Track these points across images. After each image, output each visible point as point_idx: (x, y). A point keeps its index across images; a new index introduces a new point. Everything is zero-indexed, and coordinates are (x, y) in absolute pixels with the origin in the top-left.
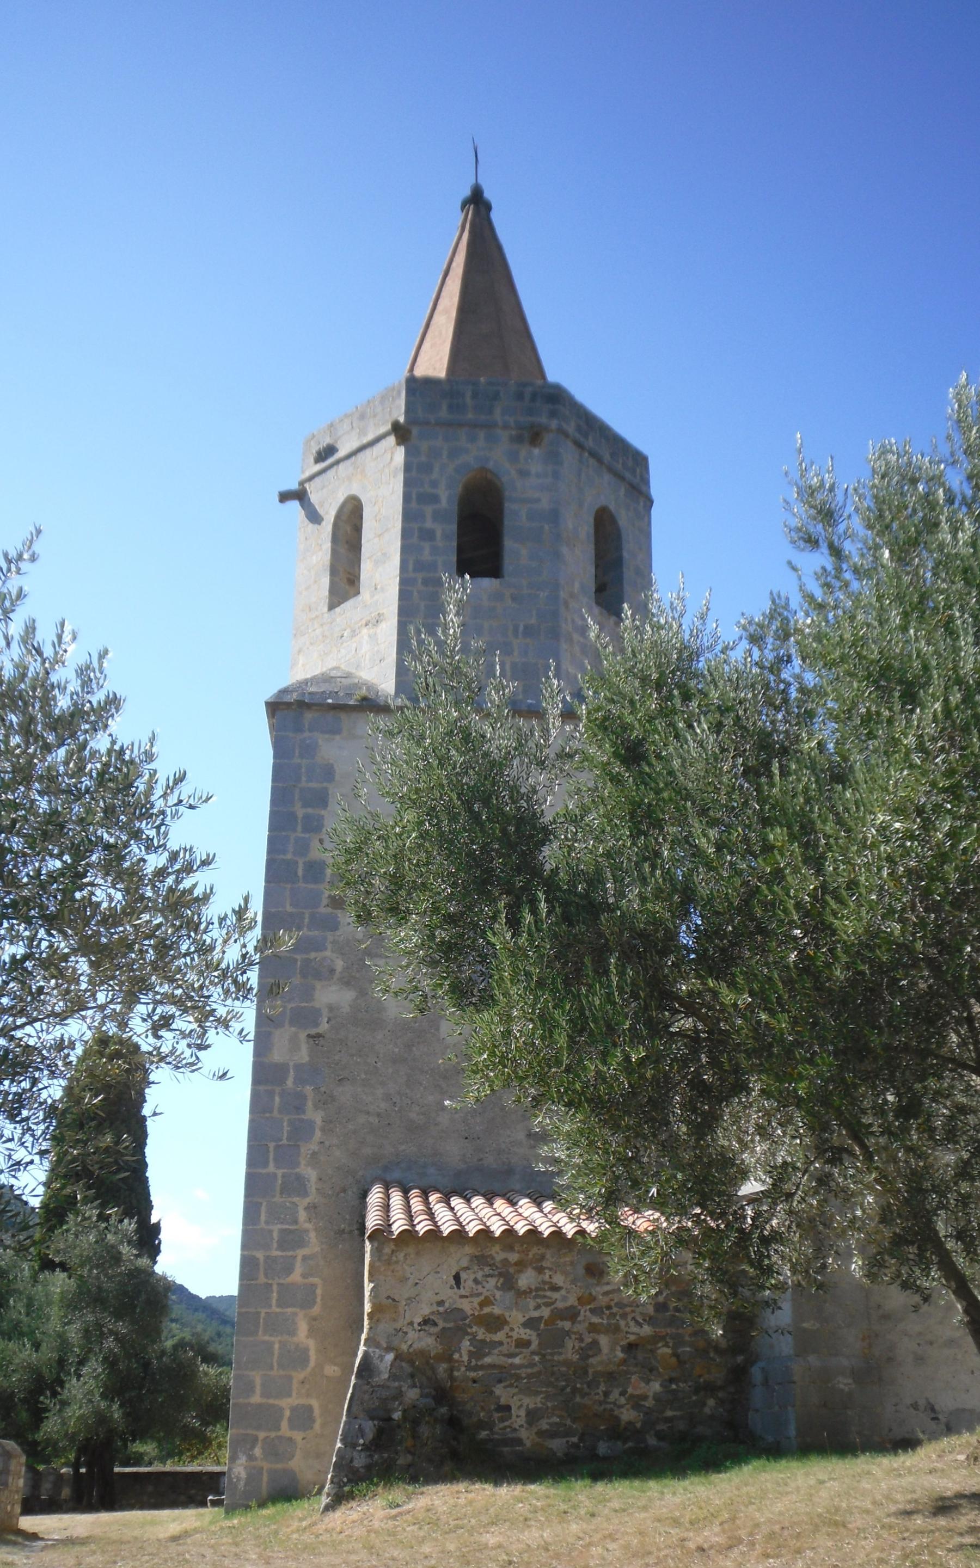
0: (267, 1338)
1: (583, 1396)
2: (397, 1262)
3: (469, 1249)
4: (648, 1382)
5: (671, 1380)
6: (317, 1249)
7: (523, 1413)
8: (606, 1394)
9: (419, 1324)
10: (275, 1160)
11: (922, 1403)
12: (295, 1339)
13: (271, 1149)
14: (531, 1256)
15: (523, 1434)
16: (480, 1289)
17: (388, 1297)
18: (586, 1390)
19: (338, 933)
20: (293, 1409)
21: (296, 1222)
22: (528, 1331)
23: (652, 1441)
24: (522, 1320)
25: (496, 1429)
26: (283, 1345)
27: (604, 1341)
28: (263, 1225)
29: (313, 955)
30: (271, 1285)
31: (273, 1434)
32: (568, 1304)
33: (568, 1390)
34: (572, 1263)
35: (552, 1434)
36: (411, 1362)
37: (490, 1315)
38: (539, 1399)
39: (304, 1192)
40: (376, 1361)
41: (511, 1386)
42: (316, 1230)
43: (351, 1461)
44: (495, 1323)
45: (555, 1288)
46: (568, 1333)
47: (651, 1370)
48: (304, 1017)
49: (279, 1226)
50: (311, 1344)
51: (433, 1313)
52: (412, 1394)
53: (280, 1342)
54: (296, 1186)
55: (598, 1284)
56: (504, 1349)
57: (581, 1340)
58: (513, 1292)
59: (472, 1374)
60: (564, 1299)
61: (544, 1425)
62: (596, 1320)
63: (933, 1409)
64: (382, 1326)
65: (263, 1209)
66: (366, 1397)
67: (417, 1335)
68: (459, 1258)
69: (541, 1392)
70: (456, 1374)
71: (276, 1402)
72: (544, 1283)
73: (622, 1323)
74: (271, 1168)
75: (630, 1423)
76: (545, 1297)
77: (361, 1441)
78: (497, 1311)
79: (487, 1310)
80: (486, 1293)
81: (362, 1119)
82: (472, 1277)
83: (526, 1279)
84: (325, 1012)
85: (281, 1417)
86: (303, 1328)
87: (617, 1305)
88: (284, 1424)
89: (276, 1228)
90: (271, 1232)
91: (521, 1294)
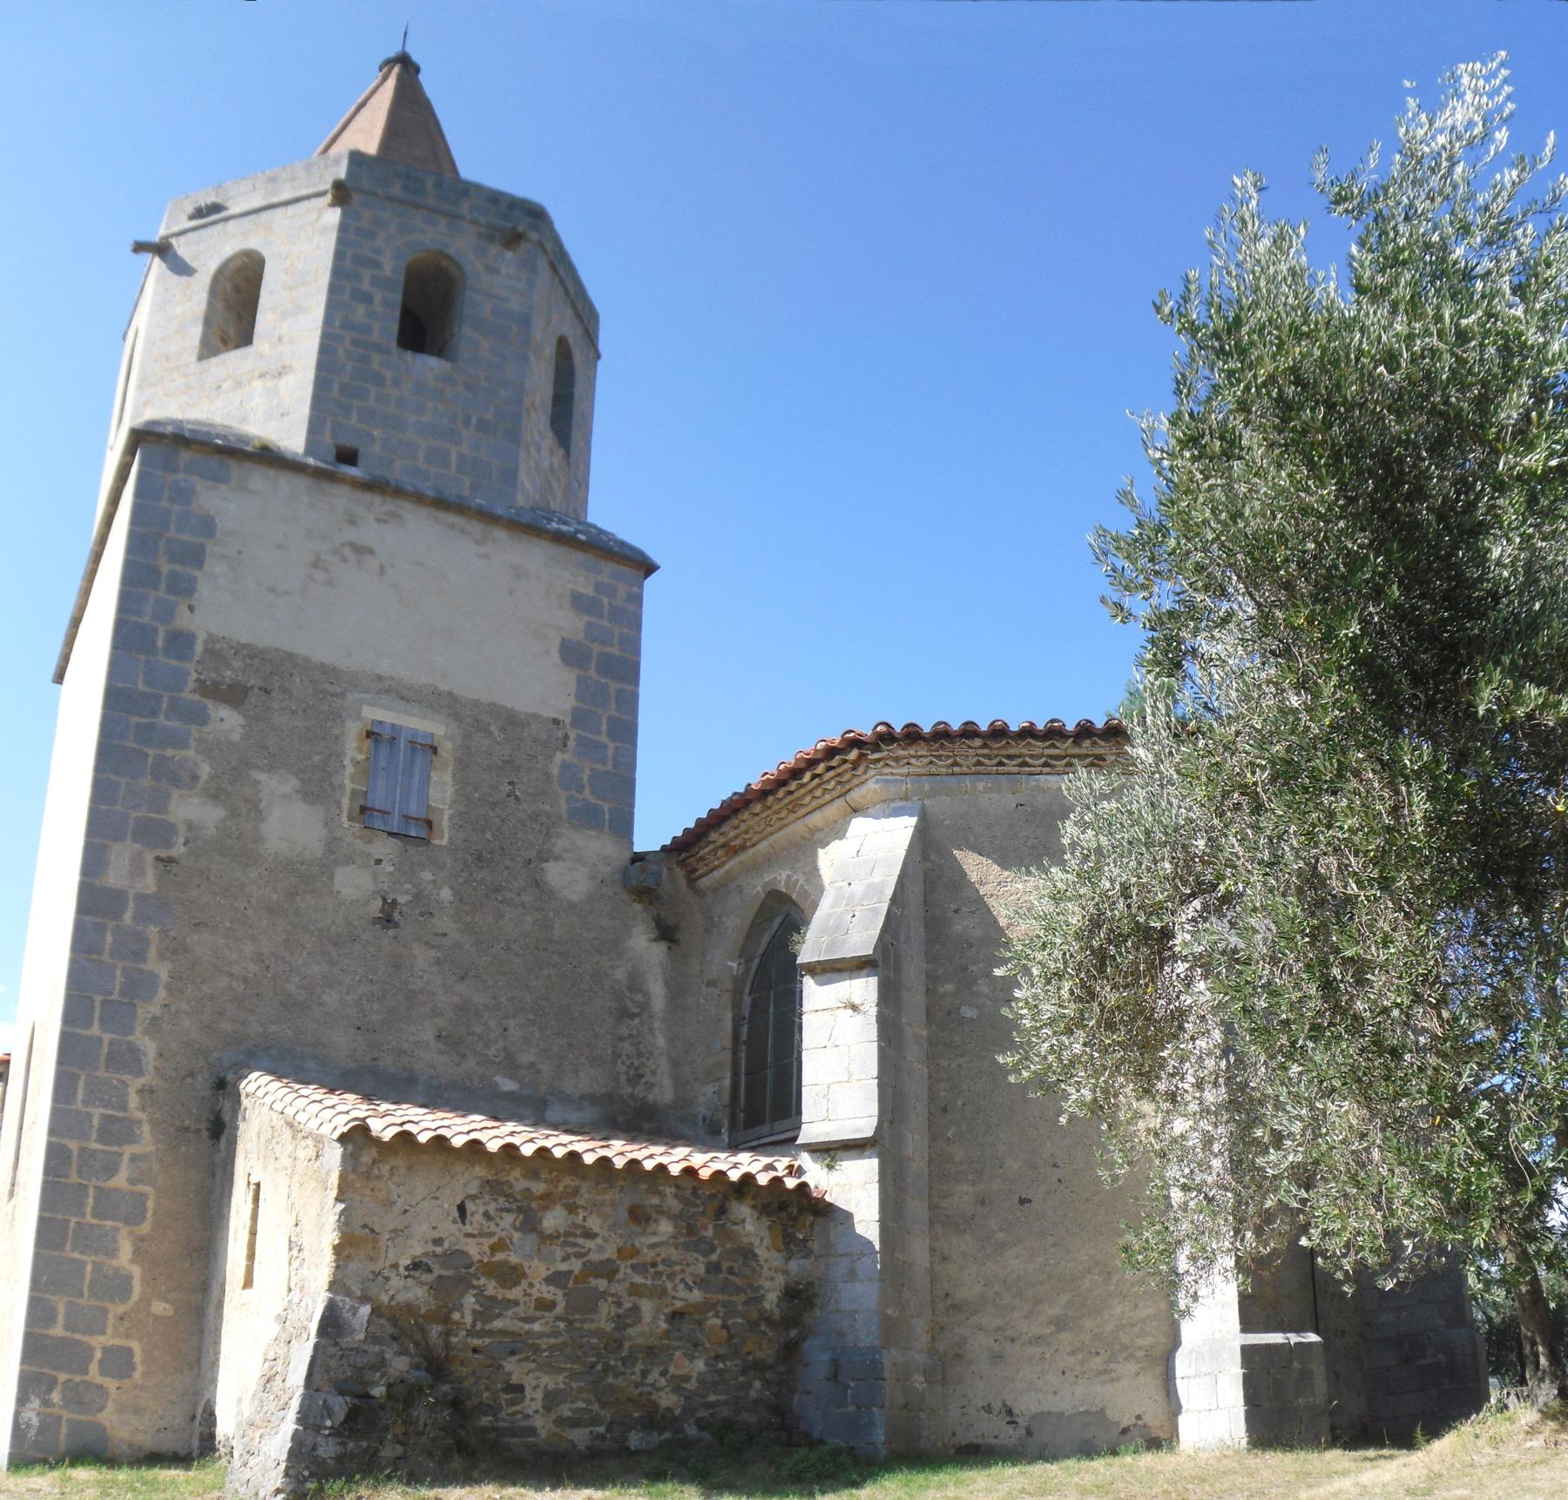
0: (76, 1255)
1: (616, 1376)
2: (379, 1177)
3: (480, 1171)
4: (692, 1358)
5: (718, 1358)
6: (151, 1148)
7: (539, 1395)
8: (644, 1374)
9: (407, 1268)
10: (101, 1020)
11: (997, 1406)
12: (114, 1262)
13: (97, 1004)
14: (561, 1188)
15: (539, 1422)
16: (493, 1228)
17: (365, 1226)
18: (622, 1369)
19: (208, 729)
20: (107, 1350)
21: (124, 1108)
22: (552, 1288)
23: (691, 1431)
24: (545, 1273)
25: (503, 1414)
26: (97, 1267)
27: (646, 1306)
28: (79, 1105)
29: (170, 752)
30: (86, 1187)
31: (78, 1378)
32: (605, 1256)
33: (599, 1367)
34: (613, 1204)
35: (574, 1423)
36: (393, 1320)
37: (504, 1263)
38: (561, 1378)
39: (139, 1072)
40: (347, 1315)
41: (527, 1359)
42: (150, 1122)
43: (314, 1448)
44: (510, 1275)
45: (590, 1235)
46: (603, 1295)
47: (695, 1345)
48: (155, 832)
49: (101, 1110)
50: (136, 1271)
51: (426, 1254)
52: (399, 1364)
53: (94, 1263)
54: (127, 1059)
55: (643, 1233)
56: (520, 1310)
57: (619, 1304)
58: (534, 1236)
59: (476, 1342)
60: (601, 1249)
61: (565, 1411)
62: (638, 1279)
63: (1010, 1412)
64: (353, 1266)
65: (81, 1085)
66: (333, 1363)
67: (402, 1283)
68: (468, 1180)
69: (565, 1370)
70: (454, 1340)
71: (84, 1338)
72: (576, 1226)
73: (669, 1285)
74: (96, 1030)
75: (669, 1409)
76: (576, 1245)
77: (328, 1423)
78: (514, 1259)
79: (500, 1256)
80: (500, 1234)
81: (223, 982)
82: (482, 1209)
83: (553, 1220)
84: (182, 830)
85: (90, 1358)
86: (126, 1250)
87: (664, 1261)
88: (94, 1368)
89: (97, 1112)
90: (89, 1116)
91: (547, 1238)
